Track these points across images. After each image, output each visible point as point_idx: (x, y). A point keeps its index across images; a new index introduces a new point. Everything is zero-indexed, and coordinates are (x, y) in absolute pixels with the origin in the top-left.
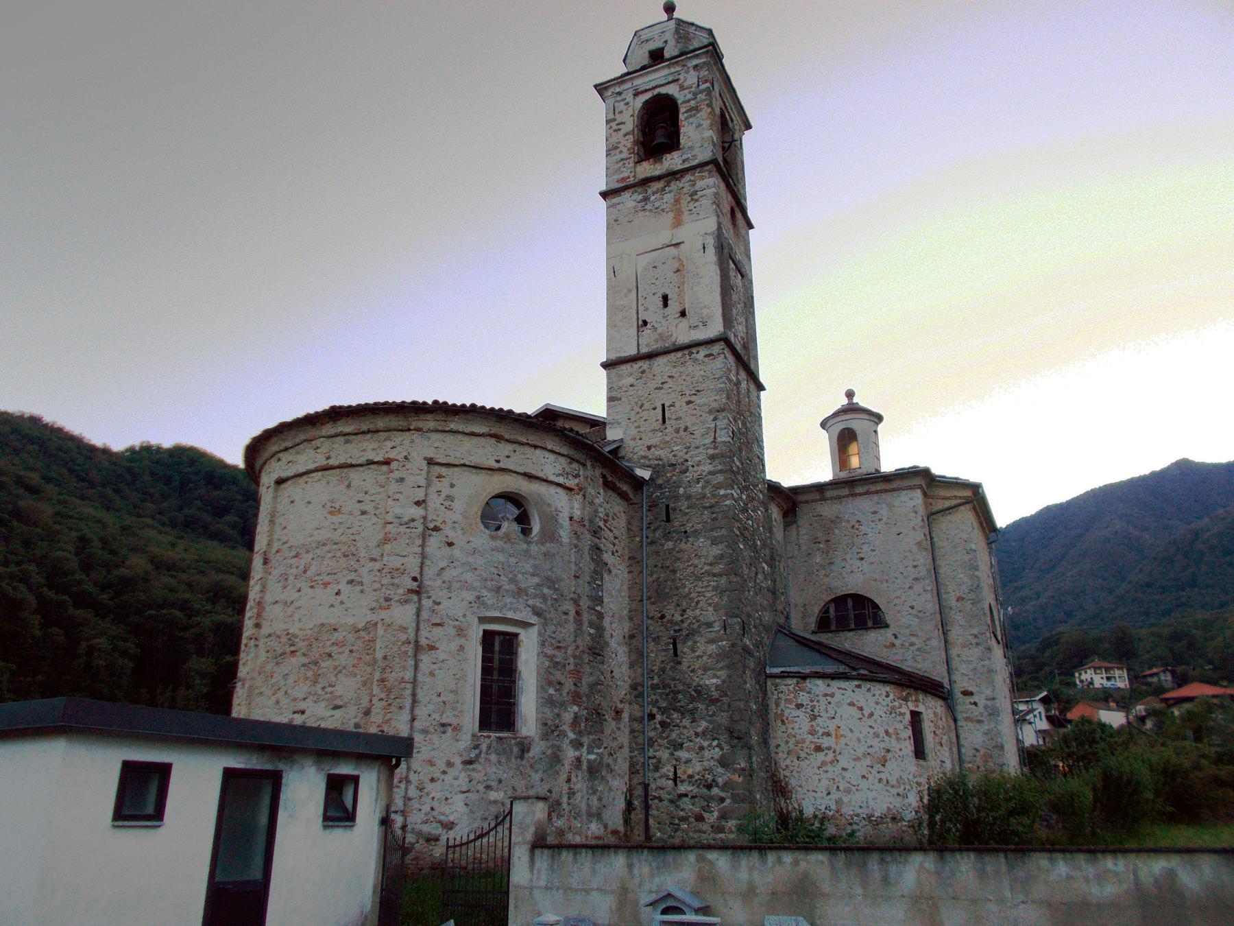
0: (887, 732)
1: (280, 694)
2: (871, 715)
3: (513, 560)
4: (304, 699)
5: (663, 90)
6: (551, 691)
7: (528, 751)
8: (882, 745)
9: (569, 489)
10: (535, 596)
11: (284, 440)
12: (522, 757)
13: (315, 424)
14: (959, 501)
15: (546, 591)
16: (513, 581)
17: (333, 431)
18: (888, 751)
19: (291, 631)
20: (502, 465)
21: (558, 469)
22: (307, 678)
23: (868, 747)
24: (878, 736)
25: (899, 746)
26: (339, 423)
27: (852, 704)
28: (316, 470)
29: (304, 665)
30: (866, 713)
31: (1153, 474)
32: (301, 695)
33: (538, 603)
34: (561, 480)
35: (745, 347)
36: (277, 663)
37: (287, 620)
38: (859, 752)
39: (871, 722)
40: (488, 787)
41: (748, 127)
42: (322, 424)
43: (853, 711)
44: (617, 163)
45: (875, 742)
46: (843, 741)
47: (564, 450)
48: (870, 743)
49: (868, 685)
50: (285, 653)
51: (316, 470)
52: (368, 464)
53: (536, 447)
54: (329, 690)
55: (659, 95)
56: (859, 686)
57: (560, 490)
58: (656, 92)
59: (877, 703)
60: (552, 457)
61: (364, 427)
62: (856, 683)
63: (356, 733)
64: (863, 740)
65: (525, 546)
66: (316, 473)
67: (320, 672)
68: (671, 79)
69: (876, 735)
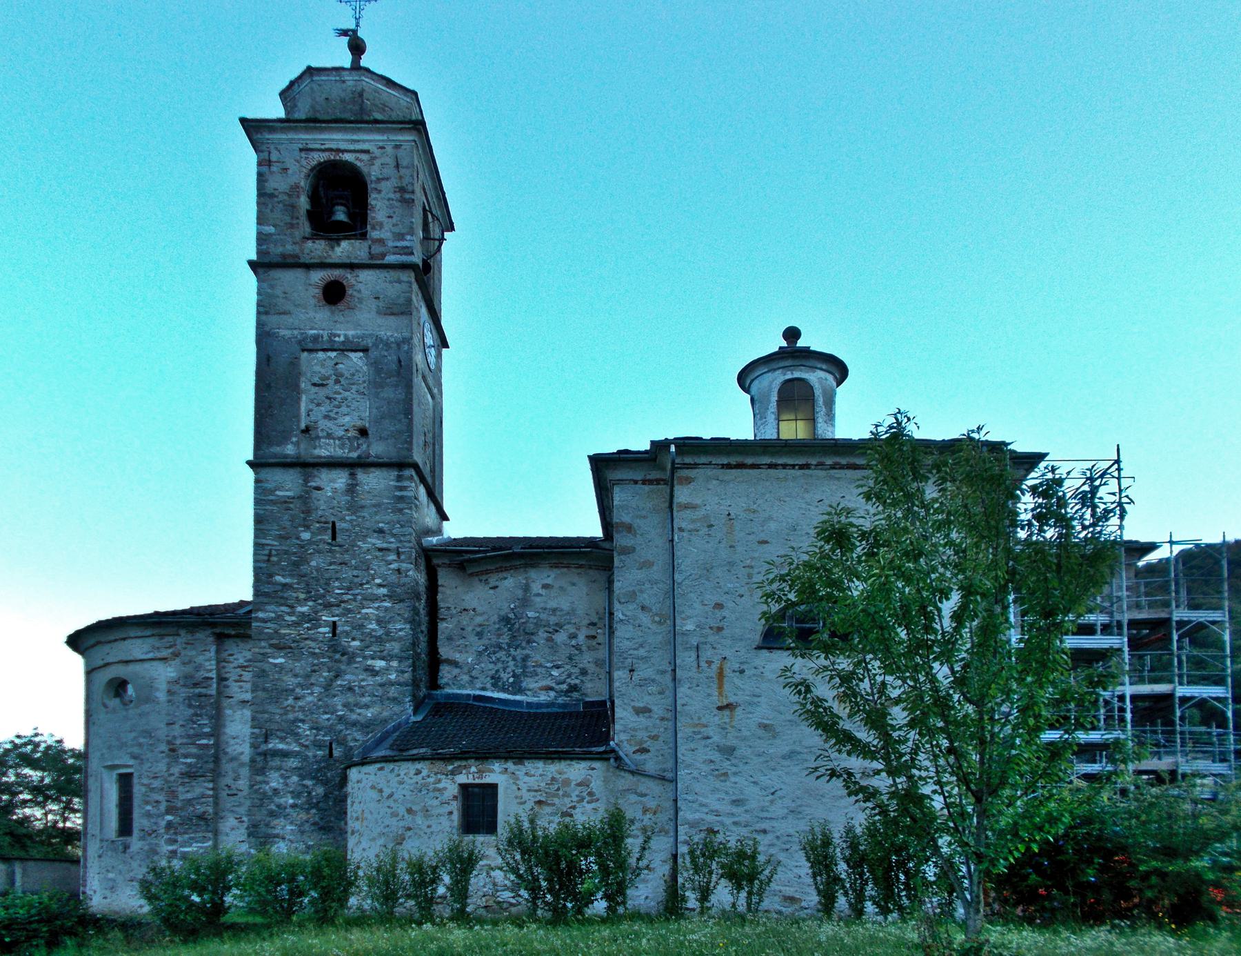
0: (410, 811)
2: (391, 796)
3: (117, 725)
6: (149, 808)
7: (129, 847)
8: (401, 824)
9: (164, 659)
10: (132, 746)
12: (124, 852)
14: (429, 480)
15: (142, 740)
16: (118, 739)
18: (409, 829)
20: (105, 661)
21: (146, 647)
23: (385, 827)
24: (397, 815)
25: (427, 823)
27: (373, 787)
30: (385, 794)
33: (136, 750)
34: (150, 656)
35: (433, 471)
38: (375, 834)
39: (391, 802)
40: (108, 871)
41: (451, 228)
43: (374, 795)
45: (394, 821)
46: (365, 823)
47: (148, 633)
48: (387, 822)
49: (391, 766)
53: (124, 639)
56: (381, 769)
57: (155, 663)
59: (401, 783)
60: (139, 641)
62: (378, 765)
63: (484, 756)
64: (380, 821)
65: (124, 713)
69: (394, 815)
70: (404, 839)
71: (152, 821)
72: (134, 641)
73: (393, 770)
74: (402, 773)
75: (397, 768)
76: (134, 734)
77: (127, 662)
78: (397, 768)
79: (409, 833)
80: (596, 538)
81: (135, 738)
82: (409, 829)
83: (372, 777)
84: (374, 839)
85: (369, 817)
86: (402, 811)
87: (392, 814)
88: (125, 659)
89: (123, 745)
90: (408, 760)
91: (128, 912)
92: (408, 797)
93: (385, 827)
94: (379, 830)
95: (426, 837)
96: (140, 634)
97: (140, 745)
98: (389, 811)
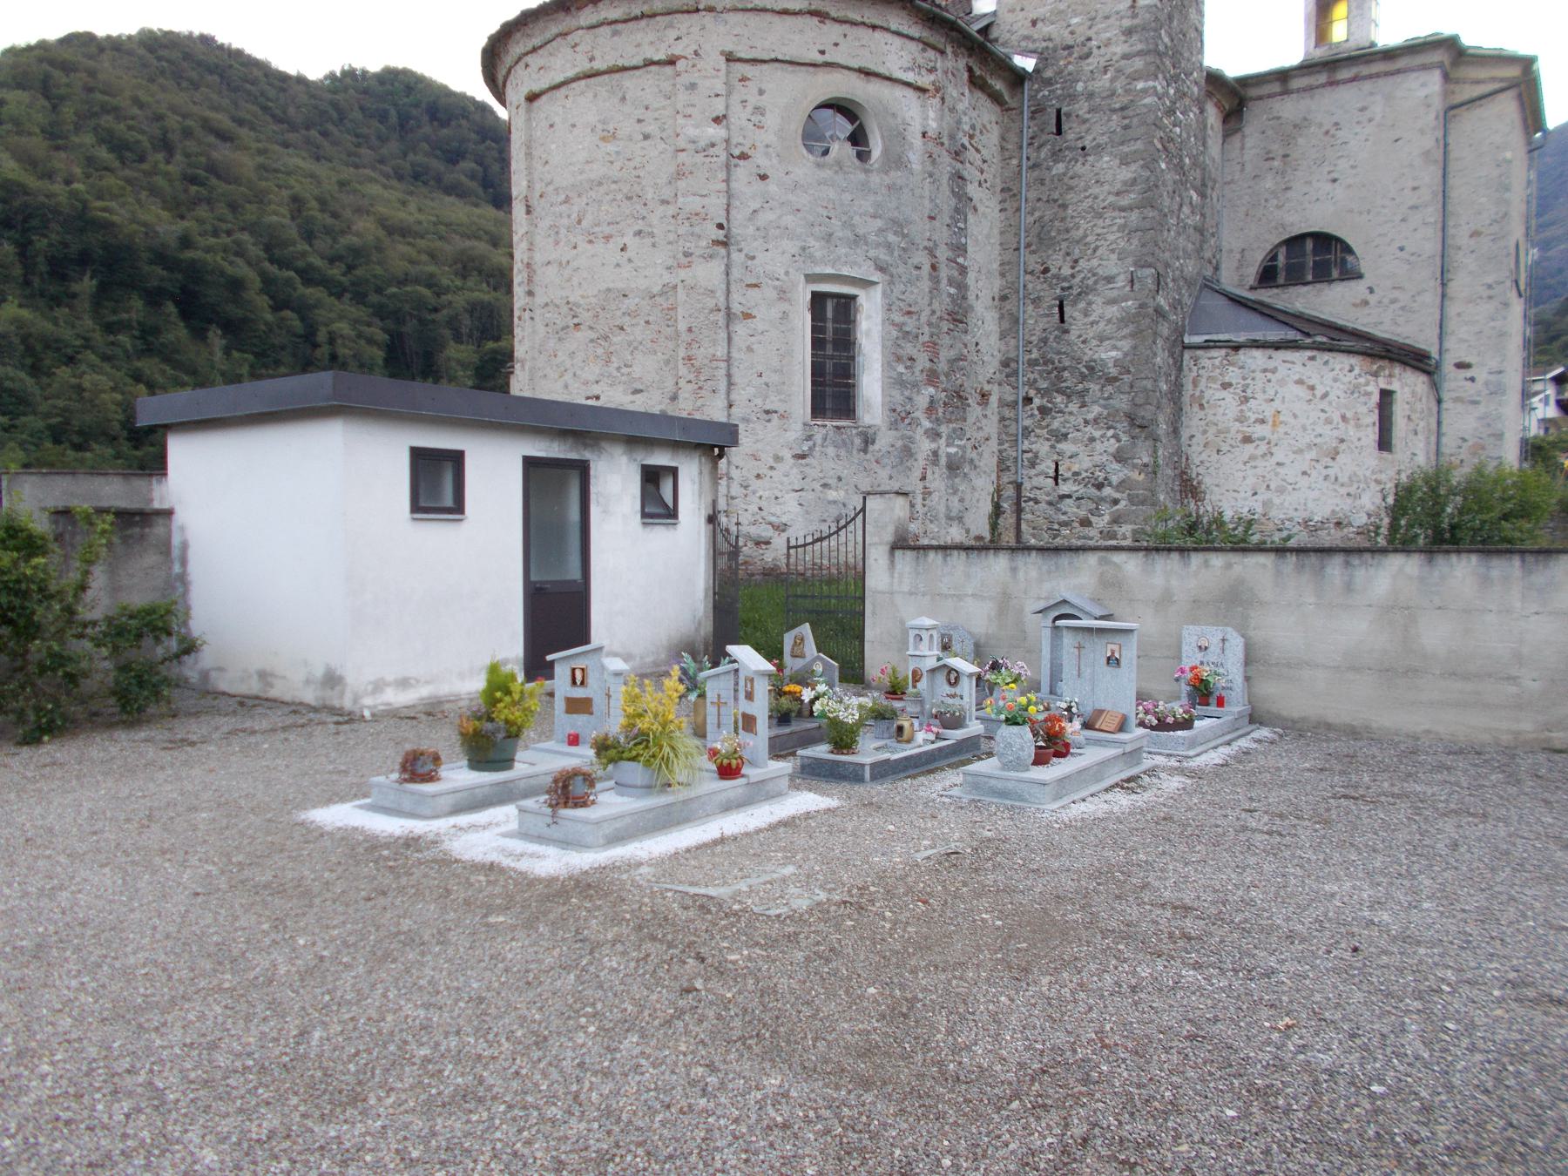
0: (1344, 418)
2: (1325, 395)
3: (847, 197)
7: (873, 442)
8: (1336, 433)
15: (891, 238)
18: (1342, 441)
20: (828, 58)
23: (1316, 436)
25: (1358, 435)
27: (1300, 382)
30: (1319, 393)
33: (882, 255)
34: (910, 77)
39: (1324, 405)
40: (825, 486)
43: (1302, 392)
45: (1326, 430)
48: (1319, 430)
49: (1326, 356)
56: (1312, 358)
59: (1335, 380)
62: (1309, 353)
65: (862, 176)
69: (1328, 421)
70: (1338, 453)
71: (907, 393)
72: (889, 37)
73: (1326, 363)
74: (1338, 367)
75: (1331, 361)
76: (879, 223)
77: (867, 73)
78: (1331, 361)
79: (1343, 446)
80: (1201, 51)
81: (881, 230)
82: (1342, 441)
83: (1298, 368)
84: (1300, 451)
85: (1292, 421)
86: (1336, 418)
87: (1326, 419)
88: (873, 67)
89: (858, 240)
90: (1343, 351)
91: (98, 739)
92: (1342, 400)
93: (1316, 436)
94: (1307, 440)
95: (1356, 451)
96: (905, 30)
97: (889, 246)
98: (1323, 416)
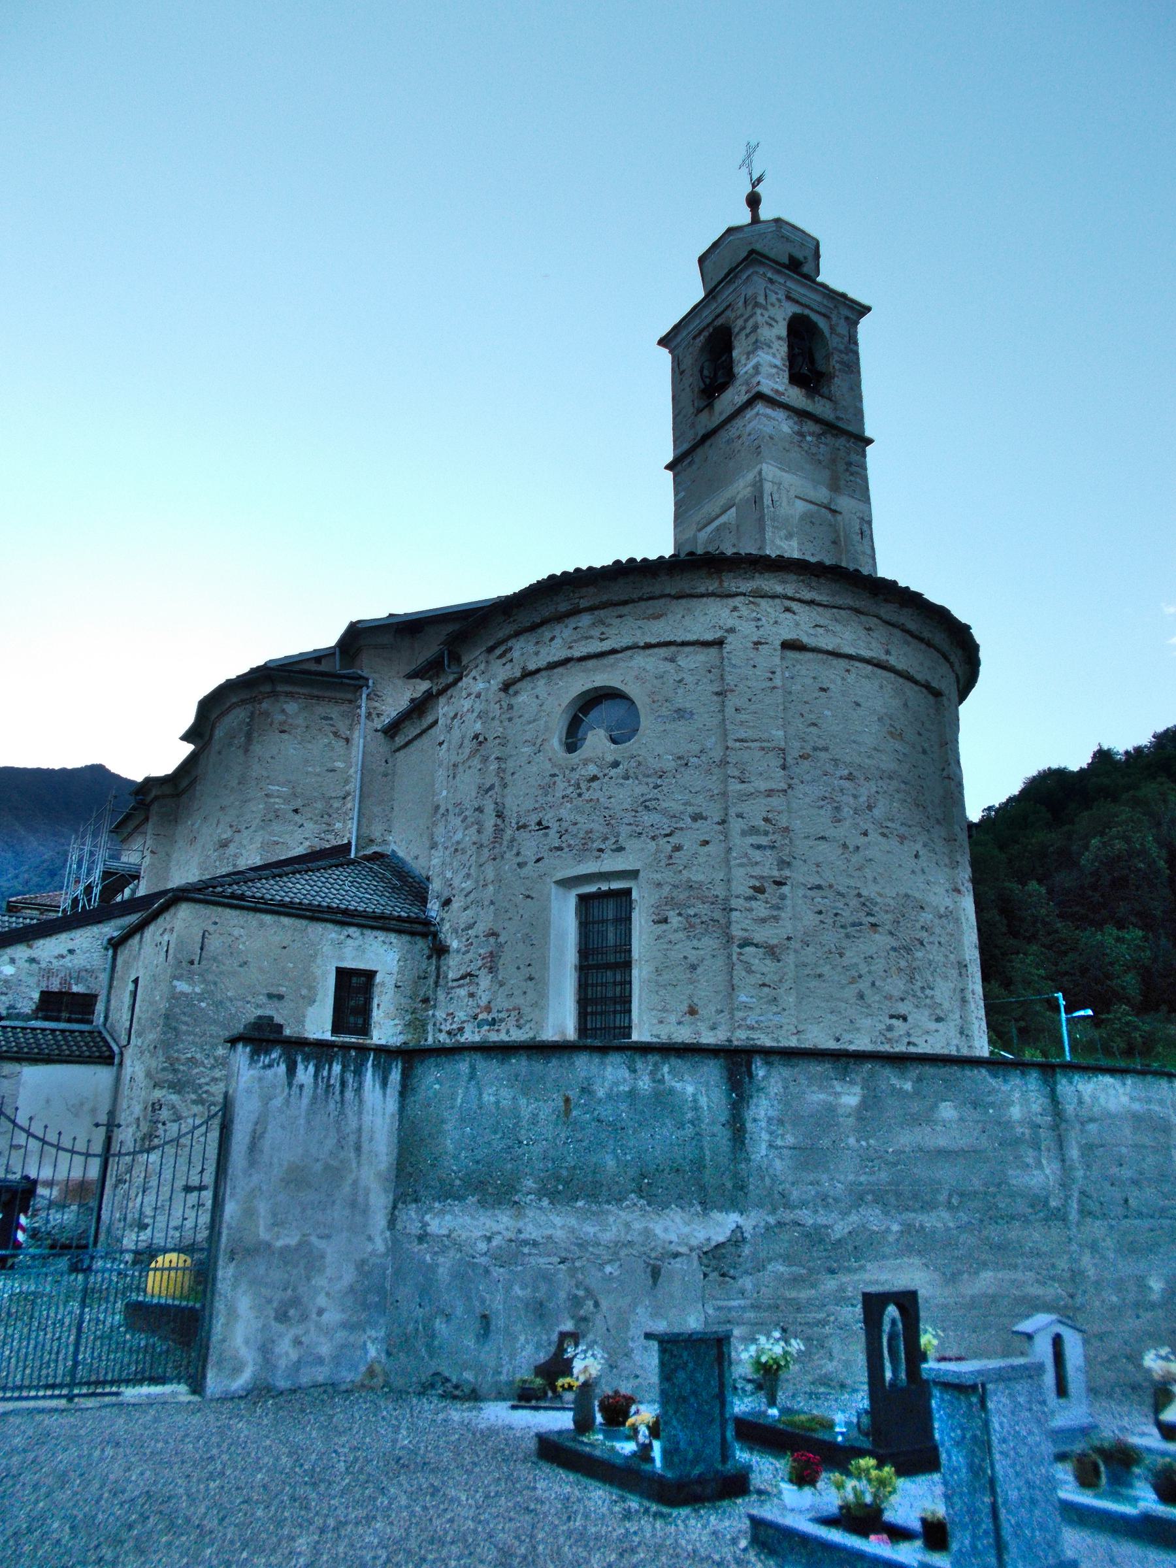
1: (864, 985)
4: (902, 1000)
5: (814, 317)
11: (784, 582)
13: (876, 595)
17: (894, 618)
19: (865, 893)
22: (900, 969)
26: (905, 610)
28: (868, 661)
29: (894, 949)
31: (63, 770)
32: (896, 994)
36: (848, 936)
37: (854, 874)
42: (886, 601)
44: (694, 338)
50: (861, 924)
51: (868, 661)
52: (923, 686)
54: (928, 992)
55: (807, 317)
58: (807, 312)
61: (926, 635)
66: (865, 665)
67: (915, 965)
68: (823, 311)
